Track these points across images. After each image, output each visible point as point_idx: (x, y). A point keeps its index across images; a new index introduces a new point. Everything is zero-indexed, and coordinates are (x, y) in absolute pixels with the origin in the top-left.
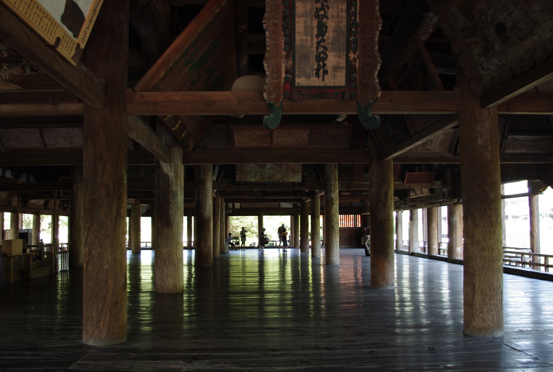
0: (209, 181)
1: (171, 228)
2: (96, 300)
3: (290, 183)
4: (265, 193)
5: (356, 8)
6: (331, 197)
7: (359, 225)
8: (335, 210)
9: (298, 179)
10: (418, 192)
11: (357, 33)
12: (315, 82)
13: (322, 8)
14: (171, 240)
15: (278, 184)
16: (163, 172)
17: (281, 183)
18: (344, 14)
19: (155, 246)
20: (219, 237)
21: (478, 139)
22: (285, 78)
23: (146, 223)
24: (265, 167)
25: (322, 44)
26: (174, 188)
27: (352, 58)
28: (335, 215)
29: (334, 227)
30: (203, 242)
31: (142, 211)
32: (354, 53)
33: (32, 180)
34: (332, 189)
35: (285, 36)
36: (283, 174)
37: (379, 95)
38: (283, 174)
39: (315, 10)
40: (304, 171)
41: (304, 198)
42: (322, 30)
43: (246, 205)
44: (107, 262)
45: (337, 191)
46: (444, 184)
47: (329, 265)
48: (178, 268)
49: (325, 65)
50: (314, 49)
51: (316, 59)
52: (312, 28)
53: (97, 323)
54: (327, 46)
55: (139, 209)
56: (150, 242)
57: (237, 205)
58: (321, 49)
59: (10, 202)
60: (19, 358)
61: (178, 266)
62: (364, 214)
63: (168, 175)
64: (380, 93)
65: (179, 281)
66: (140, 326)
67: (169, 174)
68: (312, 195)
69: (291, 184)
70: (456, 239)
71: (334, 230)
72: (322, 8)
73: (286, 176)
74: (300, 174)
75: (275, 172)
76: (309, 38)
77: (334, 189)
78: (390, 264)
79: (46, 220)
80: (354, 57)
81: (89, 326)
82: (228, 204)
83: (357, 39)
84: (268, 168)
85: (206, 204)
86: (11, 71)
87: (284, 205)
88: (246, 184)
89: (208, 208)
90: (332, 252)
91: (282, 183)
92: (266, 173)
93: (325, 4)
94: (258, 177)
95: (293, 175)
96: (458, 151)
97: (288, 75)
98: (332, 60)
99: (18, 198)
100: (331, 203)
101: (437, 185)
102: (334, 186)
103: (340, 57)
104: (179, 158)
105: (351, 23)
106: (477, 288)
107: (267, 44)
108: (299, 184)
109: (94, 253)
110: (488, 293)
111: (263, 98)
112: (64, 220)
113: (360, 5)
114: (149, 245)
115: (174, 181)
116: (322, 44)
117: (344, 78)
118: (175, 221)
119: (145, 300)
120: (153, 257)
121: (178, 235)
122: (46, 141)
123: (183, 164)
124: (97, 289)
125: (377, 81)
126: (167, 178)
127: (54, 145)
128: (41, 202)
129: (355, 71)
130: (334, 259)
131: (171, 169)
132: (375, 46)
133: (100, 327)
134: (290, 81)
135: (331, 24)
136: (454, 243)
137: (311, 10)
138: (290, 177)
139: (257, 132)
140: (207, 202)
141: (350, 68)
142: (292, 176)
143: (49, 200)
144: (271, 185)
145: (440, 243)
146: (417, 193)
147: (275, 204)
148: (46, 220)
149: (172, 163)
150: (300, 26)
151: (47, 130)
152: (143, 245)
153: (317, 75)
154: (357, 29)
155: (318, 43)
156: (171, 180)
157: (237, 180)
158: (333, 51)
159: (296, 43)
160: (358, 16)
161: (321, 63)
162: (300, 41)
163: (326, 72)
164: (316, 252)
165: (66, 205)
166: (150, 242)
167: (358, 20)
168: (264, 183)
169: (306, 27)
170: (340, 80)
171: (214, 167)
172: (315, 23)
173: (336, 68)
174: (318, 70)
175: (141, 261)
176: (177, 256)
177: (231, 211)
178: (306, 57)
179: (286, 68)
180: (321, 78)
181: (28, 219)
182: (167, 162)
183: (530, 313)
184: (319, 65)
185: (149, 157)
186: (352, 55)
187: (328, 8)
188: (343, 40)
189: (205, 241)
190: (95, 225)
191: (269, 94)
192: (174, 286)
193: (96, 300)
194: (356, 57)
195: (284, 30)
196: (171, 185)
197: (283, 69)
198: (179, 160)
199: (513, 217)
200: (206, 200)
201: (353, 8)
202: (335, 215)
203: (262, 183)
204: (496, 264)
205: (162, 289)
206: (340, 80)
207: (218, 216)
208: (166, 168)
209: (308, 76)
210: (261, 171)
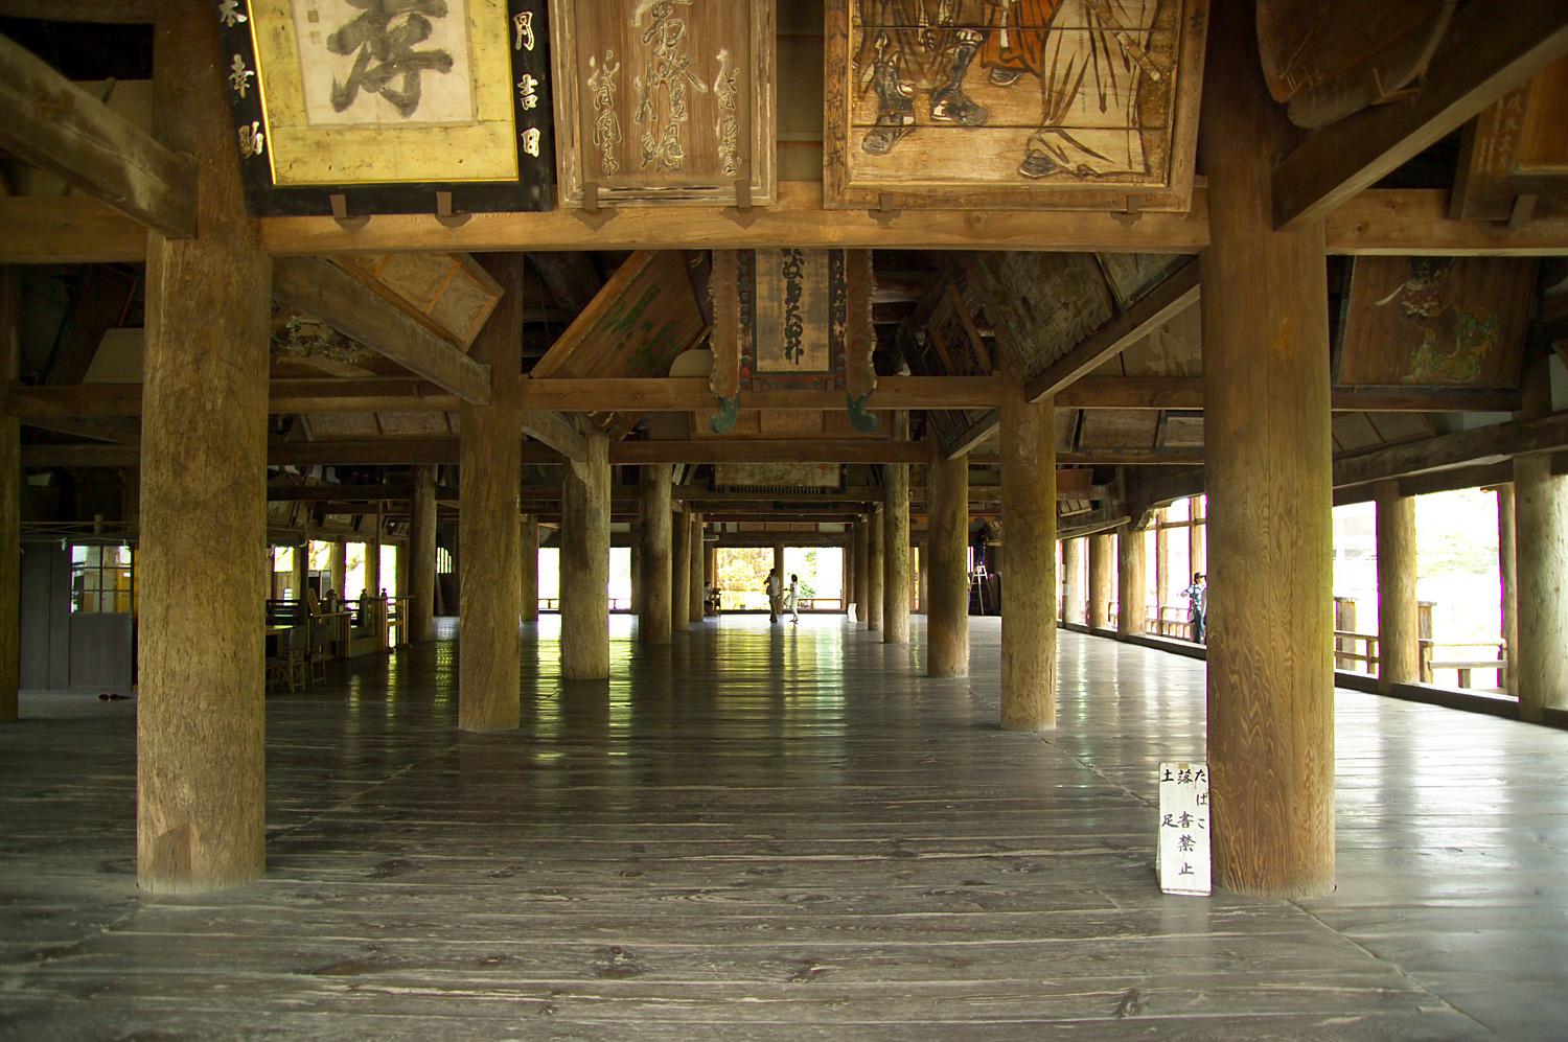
4: (777, 505)
5: (842, 263)
6: (894, 514)
9: (832, 480)
10: (1074, 506)
11: (845, 296)
12: (786, 366)
13: (794, 263)
16: (576, 477)
18: (826, 271)
19: (565, 609)
20: (688, 593)
21: (1021, 448)
22: (742, 360)
23: (549, 561)
25: (794, 313)
26: (594, 504)
27: (838, 333)
29: (899, 572)
30: (654, 597)
31: (541, 536)
32: (841, 325)
33: (332, 478)
35: (742, 302)
37: (875, 386)
39: (783, 266)
41: (860, 515)
42: (794, 293)
43: (746, 526)
44: (494, 616)
45: (907, 503)
46: (1113, 491)
49: (799, 342)
50: (784, 321)
51: (786, 334)
52: (779, 290)
54: (801, 315)
55: (536, 534)
56: (101, 609)
57: (731, 527)
58: (793, 320)
59: (295, 519)
64: (875, 383)
67: (586, 481)
68: (869, 509)
70: (1132, 599)
72: (794, 263)
73: (810, 476)
76: (776, 304)
79: (356, 551)
80: (841, 332)
83: (845, 306)
85: (659, 527)
86: (361, 352)
87: (825, 526)
88: (733, 489)
89: (663, 534)
93: (798, 257)
94: (757, 476)
96: (1081, 444)
97: (747, 357)
98: (810, 335)
99: (309, 511)
101: (1100, 492)
103: (820, 331)
105: (835, 285)
106: (1014, 661)
107: (715, 316)
108: (835, 491)
110: (1029, 668)
111: (709, 389)
112: (389, 554)
113: (848, 259)
114: (555, 605)
116: (794, 313)
117: (827, 361)
119: (548, 688)
122: (383, 424)
123: (610, 462)
125: (872, 365)
127: (396, 431)
128: (347, 519)
129: (842, 350)
132: (867, 317)
134: (750, 365)
135: (806, 285)
136: (1129, 605)
137: (778, 265)
140: (661, 523)
141: (835, 348)
143: (361, 517)
145: (1163, 609)
146: (1074, 508)
147: (809, 526)
148: (356, 551)
149: (590, 463)
150: (762, 289)
152: (542, 605)
153: (789, 356)
154: (843, 292)
155: (789, 312)
157: (718, 482)
158: (809, 323)
159: (758, 312)
160: (845, 273)
161: (794, 339)
162: (764, 308)
163: (800, 352)
165: (393, 524)
166: (101, 609)
167: (845, 280)
169: (771, 290)
170: (822, 363)
172: (784, 283)
173: (815, 347)
174: (789, 349)
177: (717, 538)
178: (771, 331)
179: (744, 346)
180: (794, 360)
181: (321, 555)
182: (582, 461)
184: (790, 342)
185: (553, 455)
186: (837, 328)
187: (802, 263)
188: (825, 307)
189: (657, 596)
190: (477, 566)
191: (718, 383)
194: (843, 330)
195: (740, 293)
197: (740, 348)
199: (1348, 552)
201: (838, 263)
204: (1041, 628)
205: (574, 672)
206: (822, 363)
207: (687, 548)
208: (581, 471)
209: (776, 359)
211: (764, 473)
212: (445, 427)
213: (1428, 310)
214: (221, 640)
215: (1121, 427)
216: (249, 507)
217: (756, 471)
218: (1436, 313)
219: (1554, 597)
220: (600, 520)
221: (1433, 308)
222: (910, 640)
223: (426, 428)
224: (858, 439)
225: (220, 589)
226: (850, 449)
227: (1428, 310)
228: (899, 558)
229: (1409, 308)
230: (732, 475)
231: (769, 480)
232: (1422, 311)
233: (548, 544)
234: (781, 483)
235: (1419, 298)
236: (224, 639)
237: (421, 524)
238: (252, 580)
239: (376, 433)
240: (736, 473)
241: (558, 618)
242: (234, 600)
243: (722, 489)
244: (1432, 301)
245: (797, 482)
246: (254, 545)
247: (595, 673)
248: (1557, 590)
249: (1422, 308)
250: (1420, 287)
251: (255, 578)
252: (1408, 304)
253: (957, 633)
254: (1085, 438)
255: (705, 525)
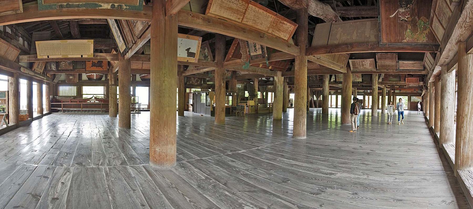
12: (255, 54)
40: (362, 77)
66: (413, 127)
74: (361, 78)
120: (38, 93)
134: (250, 54)
178: (251, 47)
183: (49, 130)
197: (248, 51)
209: (253, 53)
213: (407, 18)
215: (387, 64)
218: (410, 19)
219: (446, 110)
221: (409, 17)
222: (378, 116)
226: (326, 71)
227: (407, 18)
229: (401, 18)
232: (405, 19)
235: (404, 14)
241: (340, 109)
244: (408, 15)
248: (447, 108)
249: (405, 18)
250: (403, 11)
252: (400, 16)
254: (379, 67)
255: (392, 91)
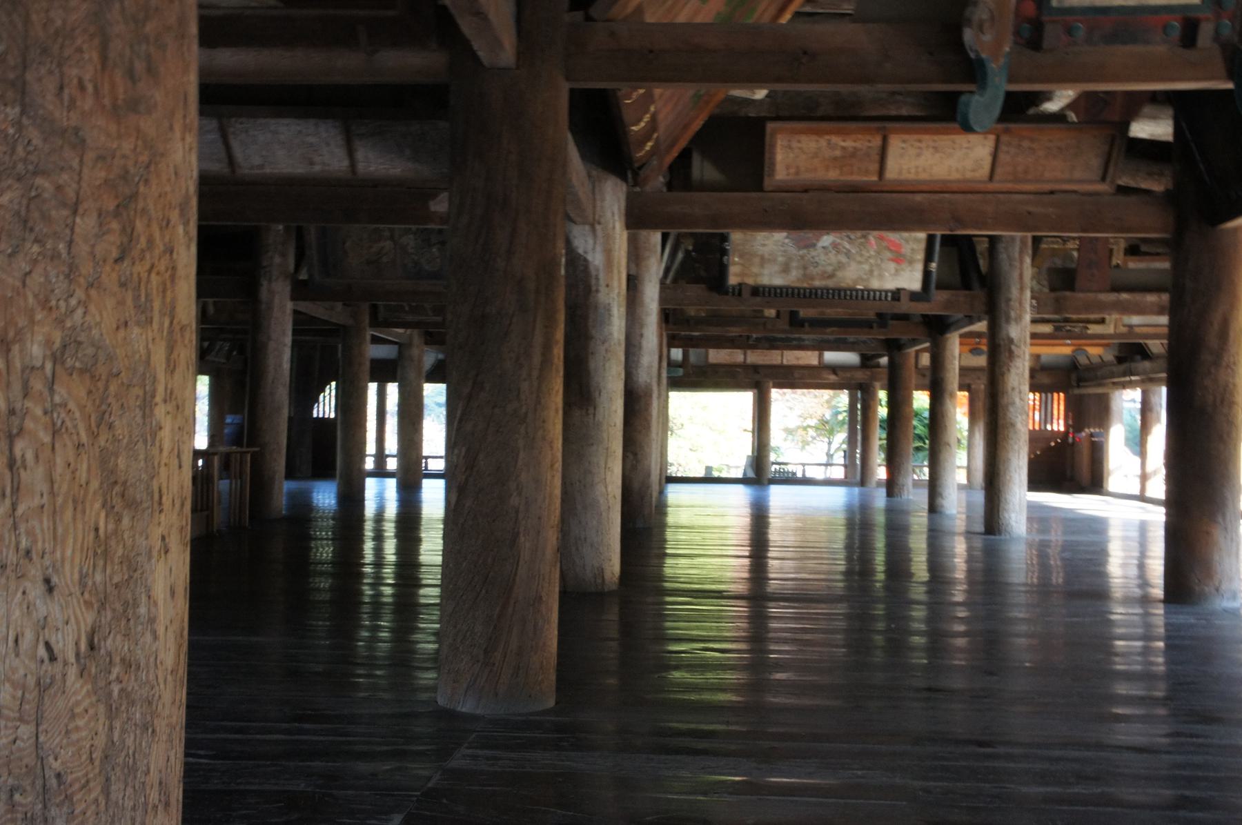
0: (651, 281)
1: (593, 411)
2: (484, 591)
3: (886, 292)
7: (1059, 425)
8: (1017, 374)
9: (911, 280)
14: (592, 444)
15: (851, 296)
17: (860, 293)
24: (814, 246)
26: (602, 297)
28: (1017, 390)
29: (1013, 425)
34: (1013, 314)
36: (866, 267)
38: (866, 267)
47: (995, 535)
48: (608, 523)
53: (486, 652)
56: (441, 457)
60: (293, 737)
61: (608, 518)
62: (1077, 391)
63: (586, 260)
65: (610, 560)
67: (590, 258)
69: (889, 294)
71: (1016, 432)
73: (876, 273)
74: (919, 267)
75: (843, 259)
77: (1018, 312)
78: (1227, 532)
81: (462, 659)
82: (688, 351)
84: (823, 247)
85: (640, 348)
88: (756, 291)
90: (1006, 499)
91: (862, 291)
92: (816, 262)
95: (897, 270)
100: (1007, 354)
102: (1017, 305)
104: (616, 211)
108: (914, 296)
109: (482, 463)
115: (601, 276)
118: (604, 392)
121: (610, 428)
124: (490, 560)
126: (582, 268)
127: (262, 166)
130: (1010, 518)
131: (595, 243)
133: (494, 664)
138: (887, 274)
139: (844, 141)
142: (893, 271)
144: (830, 296)
151: (241, 123)
156: (593, 273)
157: (733, 280)
164: (942, 498)
166: (441, 457)
168: (811, 292)
171: (665, 238)
175: (1231, 423)
176: (606, 487)
192: (597, 572)
193: (484, 591)
196: (594, 288)
198: (616, 217)
200: (642, 335)
202: (1017, 390)
203: (822, 293)
210: (802, 257)
211: (805, 268)
212: (346, 163)
214: (36, 591)
216: (151, 70)
217: (794, 264)
220: (610, 324)
223: (312, 163)
224: (1052, 192)
225: (37, 385)
228: (1013, 403)
230: (755, 270)
231: (812, 278)
233: (433, 377)
234: (830, 283)
236: (50, 588)
237: (269, 338)
238: (159, 357)
239: (226, 171)
240: (762, 265)
242: (94, 436)
243: (739, 290)
245: (856, 282)
246: (166, 224)
247: (599, 581)
251: (171, 349)
253: (1226, 529)
